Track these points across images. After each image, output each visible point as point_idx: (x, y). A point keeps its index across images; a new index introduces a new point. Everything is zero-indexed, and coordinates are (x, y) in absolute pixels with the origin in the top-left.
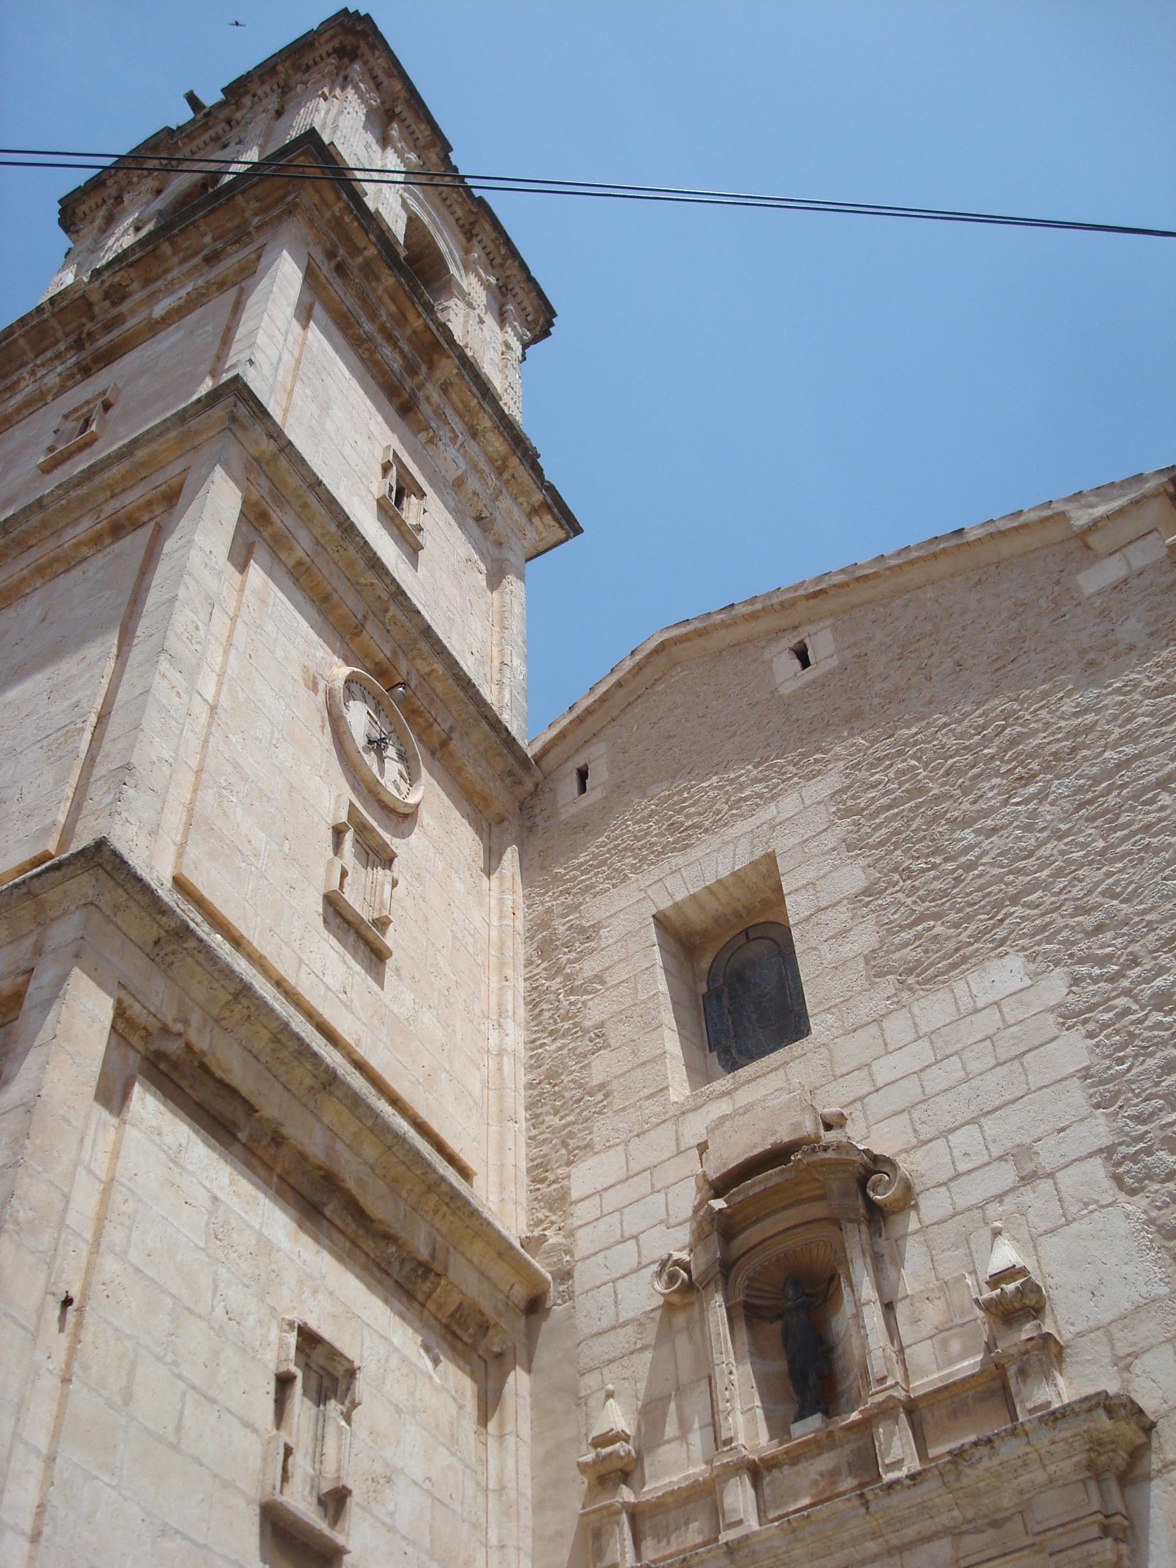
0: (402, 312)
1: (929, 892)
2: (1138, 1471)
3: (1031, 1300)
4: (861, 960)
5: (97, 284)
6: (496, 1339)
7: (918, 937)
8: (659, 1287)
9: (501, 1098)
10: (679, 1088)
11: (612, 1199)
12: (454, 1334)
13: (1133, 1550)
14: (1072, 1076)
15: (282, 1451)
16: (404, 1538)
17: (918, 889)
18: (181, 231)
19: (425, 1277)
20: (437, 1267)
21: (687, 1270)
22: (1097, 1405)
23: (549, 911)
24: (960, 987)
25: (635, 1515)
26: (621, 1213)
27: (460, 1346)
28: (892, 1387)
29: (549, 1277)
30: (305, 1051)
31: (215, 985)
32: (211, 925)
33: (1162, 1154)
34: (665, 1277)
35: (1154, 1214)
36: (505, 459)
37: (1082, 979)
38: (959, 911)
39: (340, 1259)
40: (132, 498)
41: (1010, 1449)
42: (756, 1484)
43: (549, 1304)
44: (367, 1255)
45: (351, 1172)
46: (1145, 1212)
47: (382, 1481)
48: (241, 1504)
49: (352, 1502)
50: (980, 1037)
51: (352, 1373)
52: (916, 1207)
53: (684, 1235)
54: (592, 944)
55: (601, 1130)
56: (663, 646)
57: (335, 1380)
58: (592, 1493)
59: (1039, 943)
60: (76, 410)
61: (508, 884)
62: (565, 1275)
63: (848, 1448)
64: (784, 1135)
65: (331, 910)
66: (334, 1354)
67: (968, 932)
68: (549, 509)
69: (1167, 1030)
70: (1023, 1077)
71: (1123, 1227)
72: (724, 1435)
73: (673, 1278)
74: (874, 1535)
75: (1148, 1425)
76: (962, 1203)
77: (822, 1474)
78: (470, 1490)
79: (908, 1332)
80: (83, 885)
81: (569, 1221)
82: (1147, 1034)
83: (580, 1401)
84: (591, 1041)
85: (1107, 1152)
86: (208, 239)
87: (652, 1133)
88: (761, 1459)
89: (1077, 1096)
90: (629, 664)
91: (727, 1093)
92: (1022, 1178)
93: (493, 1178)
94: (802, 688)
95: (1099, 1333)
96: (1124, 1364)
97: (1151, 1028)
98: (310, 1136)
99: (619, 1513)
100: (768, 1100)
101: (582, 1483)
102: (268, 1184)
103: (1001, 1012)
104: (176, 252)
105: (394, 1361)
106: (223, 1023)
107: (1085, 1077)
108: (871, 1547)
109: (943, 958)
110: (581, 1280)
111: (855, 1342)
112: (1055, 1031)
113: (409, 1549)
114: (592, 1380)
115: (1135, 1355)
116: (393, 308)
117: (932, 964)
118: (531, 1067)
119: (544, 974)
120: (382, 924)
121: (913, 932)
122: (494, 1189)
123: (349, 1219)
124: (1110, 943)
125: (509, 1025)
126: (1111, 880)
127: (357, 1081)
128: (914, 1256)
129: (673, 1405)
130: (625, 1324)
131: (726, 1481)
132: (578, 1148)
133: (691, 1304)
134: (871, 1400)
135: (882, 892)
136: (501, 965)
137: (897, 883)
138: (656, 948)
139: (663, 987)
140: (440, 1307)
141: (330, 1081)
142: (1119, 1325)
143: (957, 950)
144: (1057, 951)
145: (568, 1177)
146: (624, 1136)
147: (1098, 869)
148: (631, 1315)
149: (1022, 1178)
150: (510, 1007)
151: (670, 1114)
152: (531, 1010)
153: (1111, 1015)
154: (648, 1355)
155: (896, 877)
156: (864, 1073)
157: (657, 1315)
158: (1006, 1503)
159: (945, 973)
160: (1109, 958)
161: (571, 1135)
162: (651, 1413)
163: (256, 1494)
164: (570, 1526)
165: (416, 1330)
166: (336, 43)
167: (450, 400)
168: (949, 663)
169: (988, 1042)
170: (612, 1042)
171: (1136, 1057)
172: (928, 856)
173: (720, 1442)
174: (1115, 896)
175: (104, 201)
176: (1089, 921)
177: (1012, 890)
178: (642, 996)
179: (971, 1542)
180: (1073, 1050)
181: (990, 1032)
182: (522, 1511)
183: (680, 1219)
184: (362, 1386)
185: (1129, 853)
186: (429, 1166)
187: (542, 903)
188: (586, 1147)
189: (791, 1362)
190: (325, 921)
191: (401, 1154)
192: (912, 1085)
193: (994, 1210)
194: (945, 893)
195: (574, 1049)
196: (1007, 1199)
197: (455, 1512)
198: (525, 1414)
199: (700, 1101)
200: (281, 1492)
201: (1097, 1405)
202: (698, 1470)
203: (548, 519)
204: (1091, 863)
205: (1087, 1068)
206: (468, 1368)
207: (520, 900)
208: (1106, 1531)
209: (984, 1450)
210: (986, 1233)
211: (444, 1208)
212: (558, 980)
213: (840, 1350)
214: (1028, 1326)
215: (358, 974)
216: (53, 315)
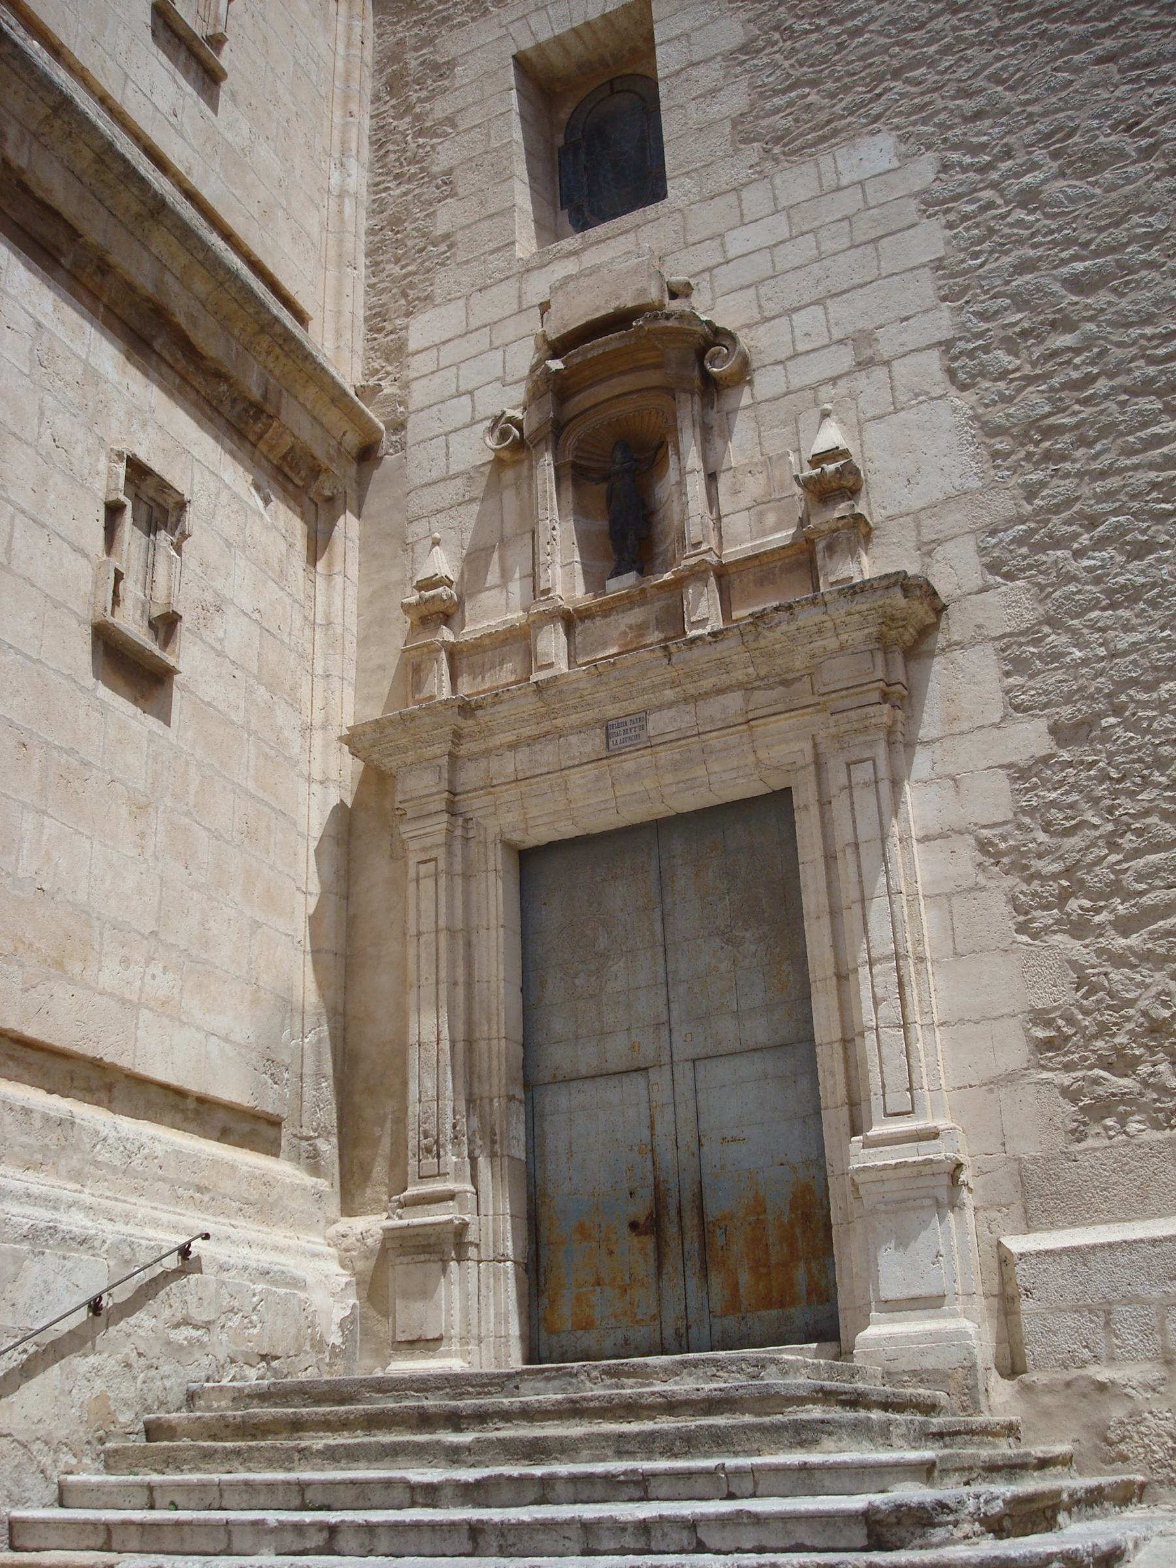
1: (810, 56)
2: (924, 648)
3: (849, 482)
4: (728, 125)
6: (327, 484)
7: (790, 104)
8: (491, 442)
9: (341, 242)
10: (526, 245)
12: (286, 476)
13: (908, 718)
14: (924, 266)
15: (112, 575)
16: (233, 663)
17: (797, 52)
19: (257, 418)
20: (269, 409)
21: (520, 429)
22: (895, 584)
23: (401, 43)
24: (826, 162)
25: (453, 653)
26: (460, 370)
27: (291, 487)
28: (705, 552)
29: (382, 426)
30: (130, 174)
31: (33, 96)
32: (28, 30)
33: (999, 353)
34: (497, 433)
37: (953, 166)
38: (838, 79)
39: (170, 394)
41: (808, 617)
42: (569, 632)
43: (381, 452)
44: (198, 392)
45: (181, 306)
46: (972, 408)
47: (212, 609)
48: (74, 623)
49: (182, 627)
50: (839, 216)
51: (182, 506)
52: (750, 383)
53: (519, 394)
54: (446, 82)
55: (443, 281)
57: (165, 512)
58: (413, 632)
59: (914, 124)
61: (358, 9)
62: (399, 426)
63: (658, 605)
64: (628, 300)
65: (160, 22)
66: (164, 486)
67: (843, 104)
69: (1028, 228)
70: (875, 263)
71: (948, 419)
72: (543, 586)
73: (504, 434)
74: (673, 684)
75: (940, 606)
76: (796, 382)
77: (630, 627)
78: (298, 622)
79: (730, 497)
81: (404, 373)
82: (1007, 231)
83: (407, 547)
84: (438, 187)
85: (946, 345)
87: (494, 289)
88: (575, 610)
89: (926, 286)
91: (575, 253)
92: (859, 364)
93: (330, 325)
95: (908, 518)
96: (927, 549)
97: (1011, 226)
98: (138, 267)
99: (439, 651)
100: (615, 264)
101: (405, 623)
102: (94, 313)
103: (864, 192)
105: (225, 497)
106: (42, 139)
107: (938, 269)
108: (669, 694)
109: (812, 130)
110: (416, 429)
111: (676, 508)
112: (915, 217)
113: (237, 673)
114: (420, 528)
115: (939, 542)
117: (802, 135)
118: (373, 211)
119: (392, 112)
120: (217, 41)
121: (786, 98)
122: (329, 335)
123: (179, 355)
124: (988, 131)
125: (352, 165)
126: (999, 65)
127: (187, 212)
128: (743, 431)
129: (496, 556)
131: (541, 628)
132: (418, 299)
133: (521, 461)
134: (684, 563)
135: (758, 51)
136: (347, 99)
137: (776, 43)
138: (514, 92)
139: (517, 134)
140: (272, 448)
141: (159, 208)
142: (928, 512)
143: (829, 122)
144: (932, 134)
145: (407, 328)
146: (465, 290)
147: (989, 51)
148: (461, 468)
149: (859, 364)
150: (354, 146)
151: (515, 270)
152: (377, 150)
153: (974, 207)
154: (476, 507)
155: (777, 36)
157: (487, 470)
158: (798, 665)
159: (813, 145)
160: (983, 147)
161: (411, 285)
162: (475, 561)
163: (88, 616)
164: (392, 662)
165: (247, 469)
169: (845, 223)
170: (460, 190)
171: (991, 252)
172: (813, 16)
173: (538, 592)
174: (1000, 82)
176: (969, 106)
177: (895, 63)
178: (495, 144)
179: (759, 697)
180: (930, 240)
181: (849, 212)
182: (347, 645)
183: (515, 378)
184: (192, 519)
185: (1023, 37)
186: (262, 306)
187: (394, 33)
188: (426, 298)
189: (612, 523)
190: (154, 34)
191: (233, 291)
192: (763, 260)
193: (826, 392)
194: (825, 59)
195: (420, 195)
196: (840, 383)
197: (282, 642)
198: (354, 556)
199: (547, 258)
200: (113, 614)
201: (895, 584)
202: (516, 616)
204: (982, 43)
205: (940, 259)
206: (298, 509)
207: (370, 27)
208: (885, 697)
209: (784, 615)
210: (815, 414)
211: (278, 350)
212: (408, 119)
213: (661, 514)
214: (842, 506)
215: (190, 95)
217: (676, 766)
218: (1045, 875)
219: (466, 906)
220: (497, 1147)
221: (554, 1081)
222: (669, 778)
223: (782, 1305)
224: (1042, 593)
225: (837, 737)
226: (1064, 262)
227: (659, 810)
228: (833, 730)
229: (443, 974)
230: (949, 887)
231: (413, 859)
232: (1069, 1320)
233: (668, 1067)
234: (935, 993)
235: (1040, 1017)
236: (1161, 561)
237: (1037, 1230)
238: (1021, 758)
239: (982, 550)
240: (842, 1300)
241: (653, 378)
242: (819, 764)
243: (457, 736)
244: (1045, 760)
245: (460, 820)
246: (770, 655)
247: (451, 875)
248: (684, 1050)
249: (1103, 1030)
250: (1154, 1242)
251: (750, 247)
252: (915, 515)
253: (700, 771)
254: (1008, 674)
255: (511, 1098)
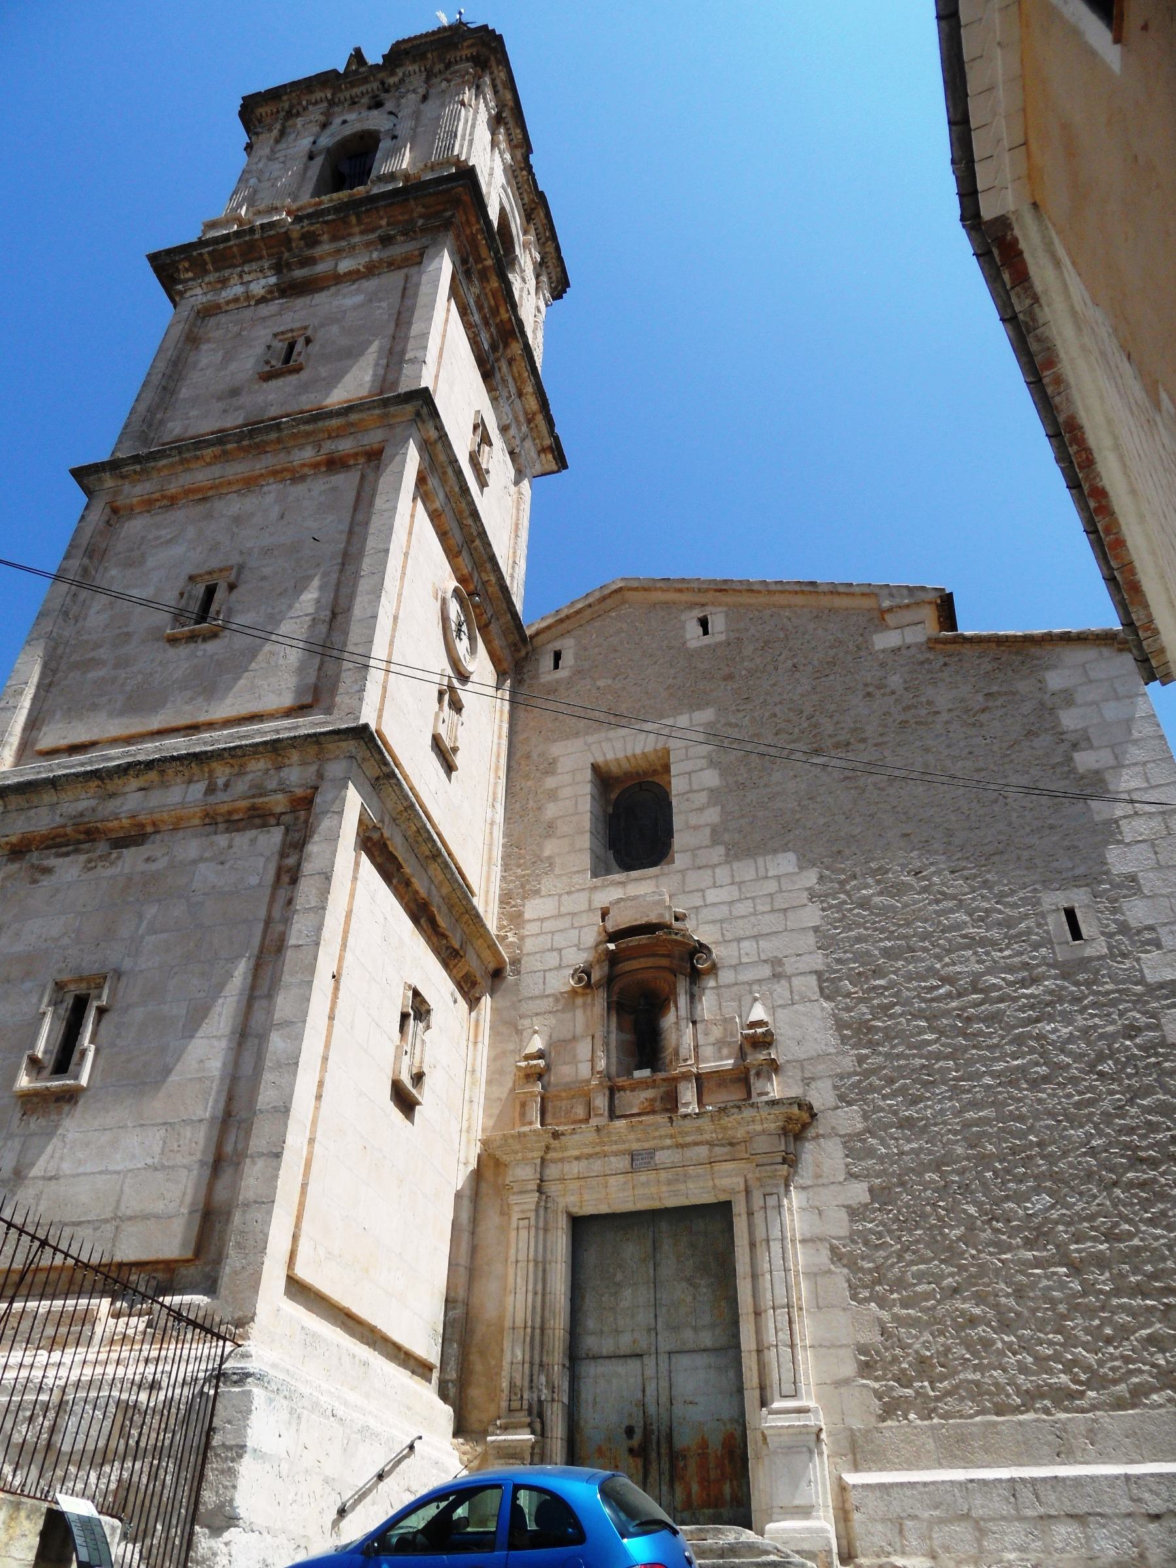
0: (497, 307)
5: (298, 227)
11: (548, 926)
18: (367, 211)
19: (455, 957)
20: (461, 953)
35: (845, 1015)
36: (534, 414)
40: (345, 446)
52: (716, 974)
56: (620, 589)
60: (283, 333)
63: (662, 1089)
66: (424, 1001)
68: (552, 452)
74: (672, 1137)
79: (699, 1035)
80: (350, 746)
83: (519, 1032)
85: (819, 974)
86: (384, 222)
89: (811, 939)
90: (597, 595)
94: (701, 648)
96: (807, 1082)
97: (855, 915)
104: (359, 222)
108: (668, 1142)
110: (527, 964)
112: (806, 901)
115: (813, 1079)
116: (492, 302)
120: (455, 750)
130: (548, 996)
145: (523, 905)
156: (700, 894)
158: (739, 1136)
160: (843, 871)
166: (474, 51)
167: (511, 370)
168: (789, 663)
175: (278, 112)
179: (718, 1150)
180: (812, 915)
192: (735, 913)
193: (755, 987)
203: (550, 457)
209: (736, 1110)
210: (749, 998)
216: (262, 238)
217: (669, 1183)
218: (864, 1268)
219: (545, 1247)
220: (555, 1395)
221: (587, 1357)
222: (664, 1188)
223: (716, 1506)
224: (865, 1117)
225: (759, 1179)
226: (881, 940)
227: (656, 1205)
228: (758, 1175)
229: (530, 1287)
230: (815, 1269)
231: (515, 1217)
232: (880, 1527)
233: (653, 1357)
234: (807, 1329)
235: (862, 1349)
236: (926, 1107)
237: (860, 1471)
238: (853, 1203)
239: (836, 1087)
240: (754, 1505)
241: (665, 962)
242: (748, 1192)
243: (548, 1148)
244: (866, 1205)
245: (544, 1197)
246: (725, 1129)
247: (537, 1228)
248: (664, 1346)
249: (895, 1360)
250: (925, 1484)
251: (718, 900)
252: (801, 1063)
253: (682, 1187)
254: (847, 1156)
255: (564, 1366)
